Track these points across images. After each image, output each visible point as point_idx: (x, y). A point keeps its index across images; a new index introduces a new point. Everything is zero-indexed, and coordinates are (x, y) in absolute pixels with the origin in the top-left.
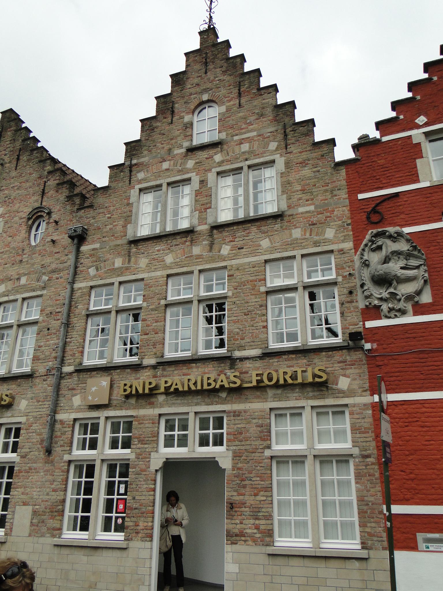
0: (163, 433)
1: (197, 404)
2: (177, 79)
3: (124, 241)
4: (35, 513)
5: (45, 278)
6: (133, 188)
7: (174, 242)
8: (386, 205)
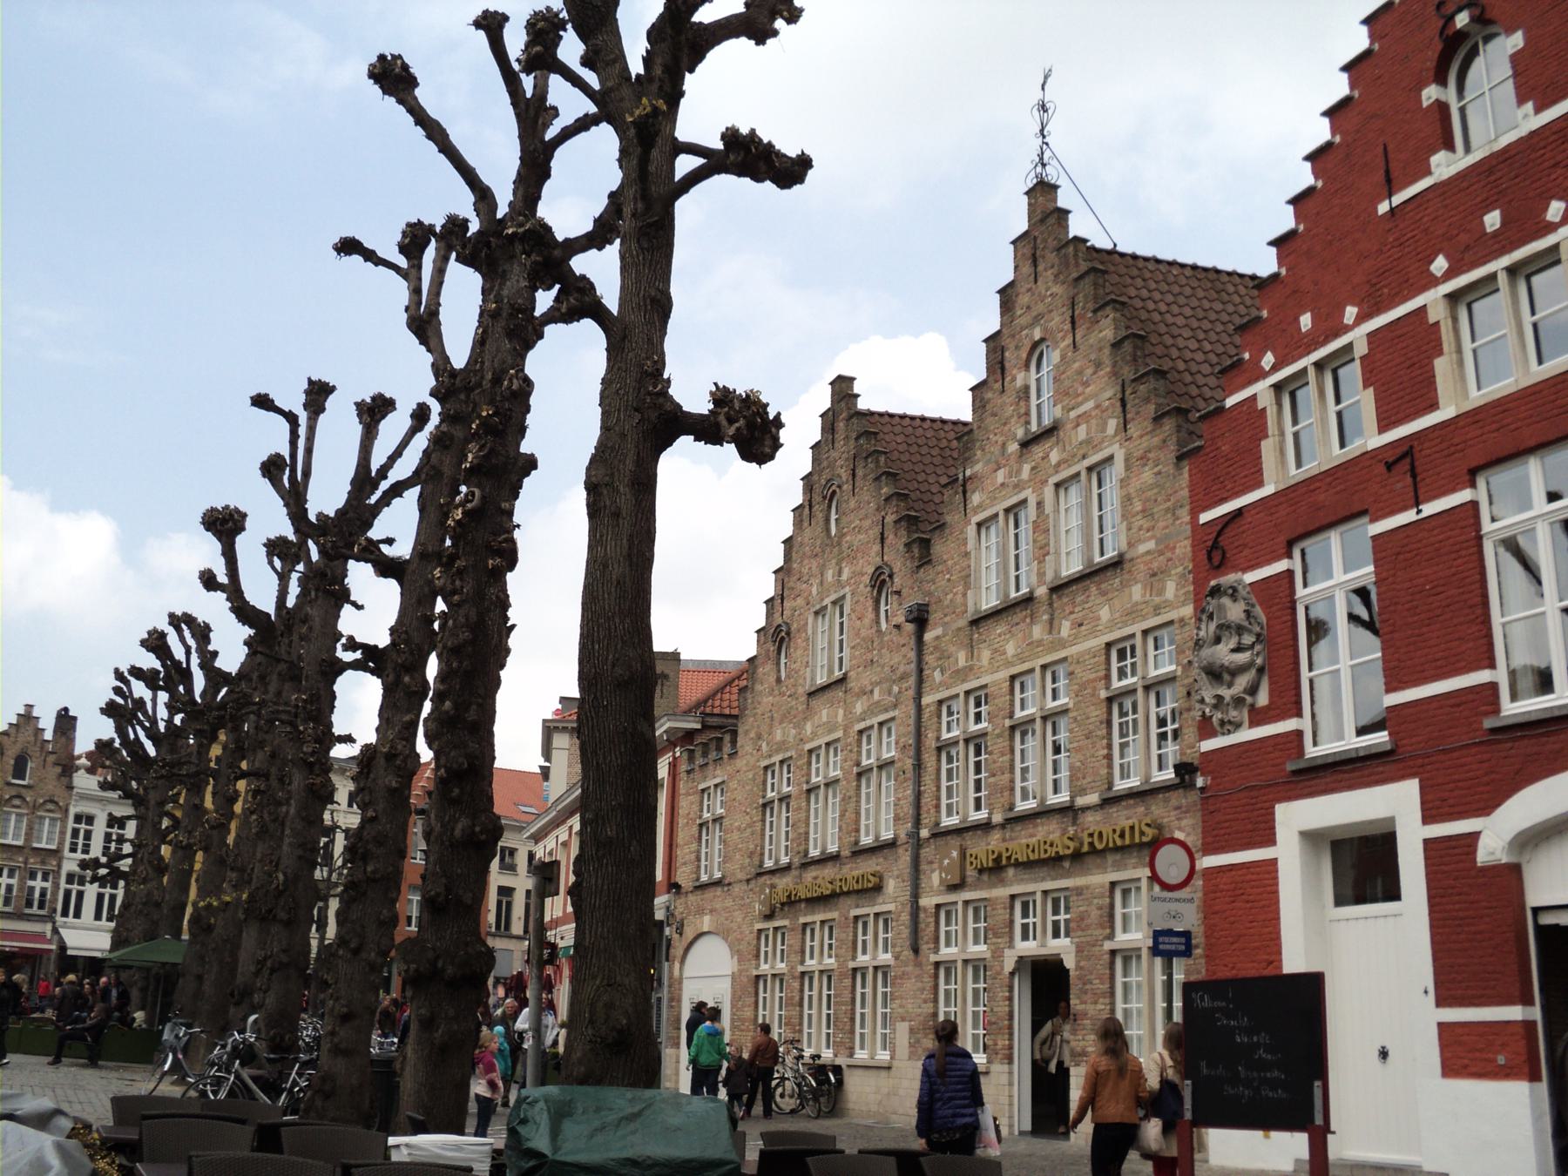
0: (1019, 921)
1: (1043, 879)
2: (1007, 295)
3: (962, 623)
4: (912, 1030)
5: (896, 689)
6: (969, 523)
7: (1016, 619)
8: (1229, 532)
